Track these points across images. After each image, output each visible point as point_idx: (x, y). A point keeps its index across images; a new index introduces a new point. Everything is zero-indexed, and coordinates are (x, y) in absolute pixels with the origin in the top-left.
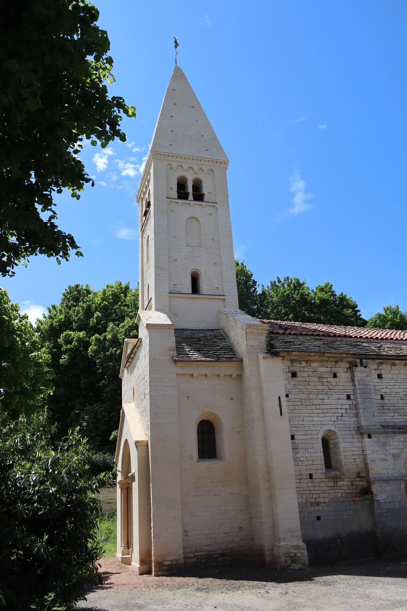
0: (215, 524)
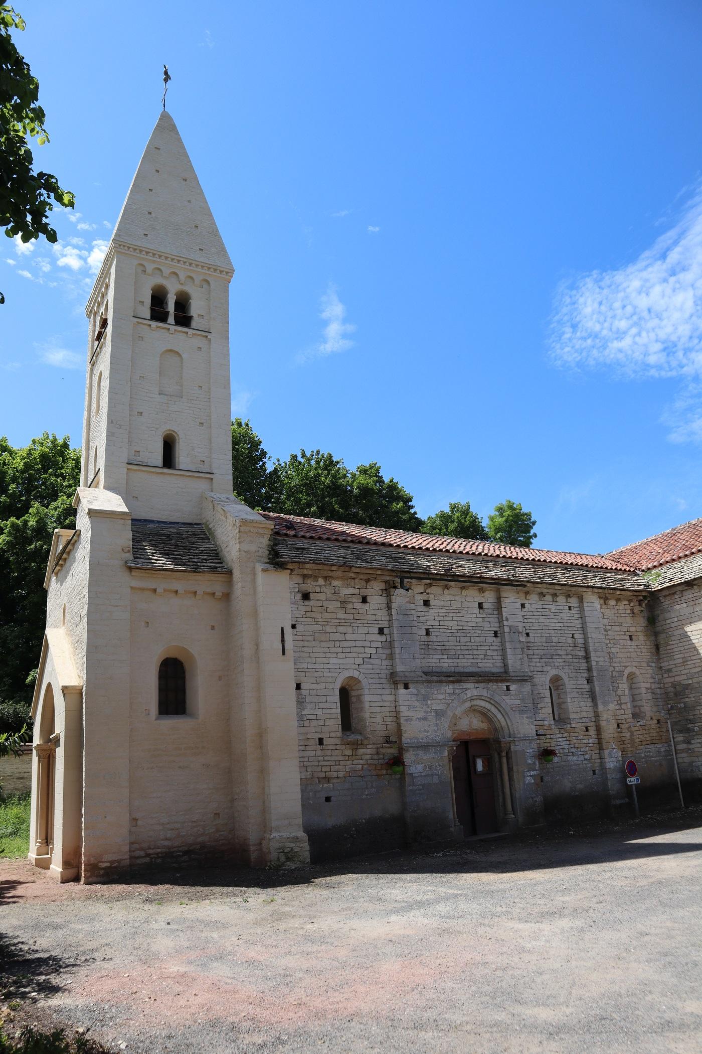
0: (178, 809)
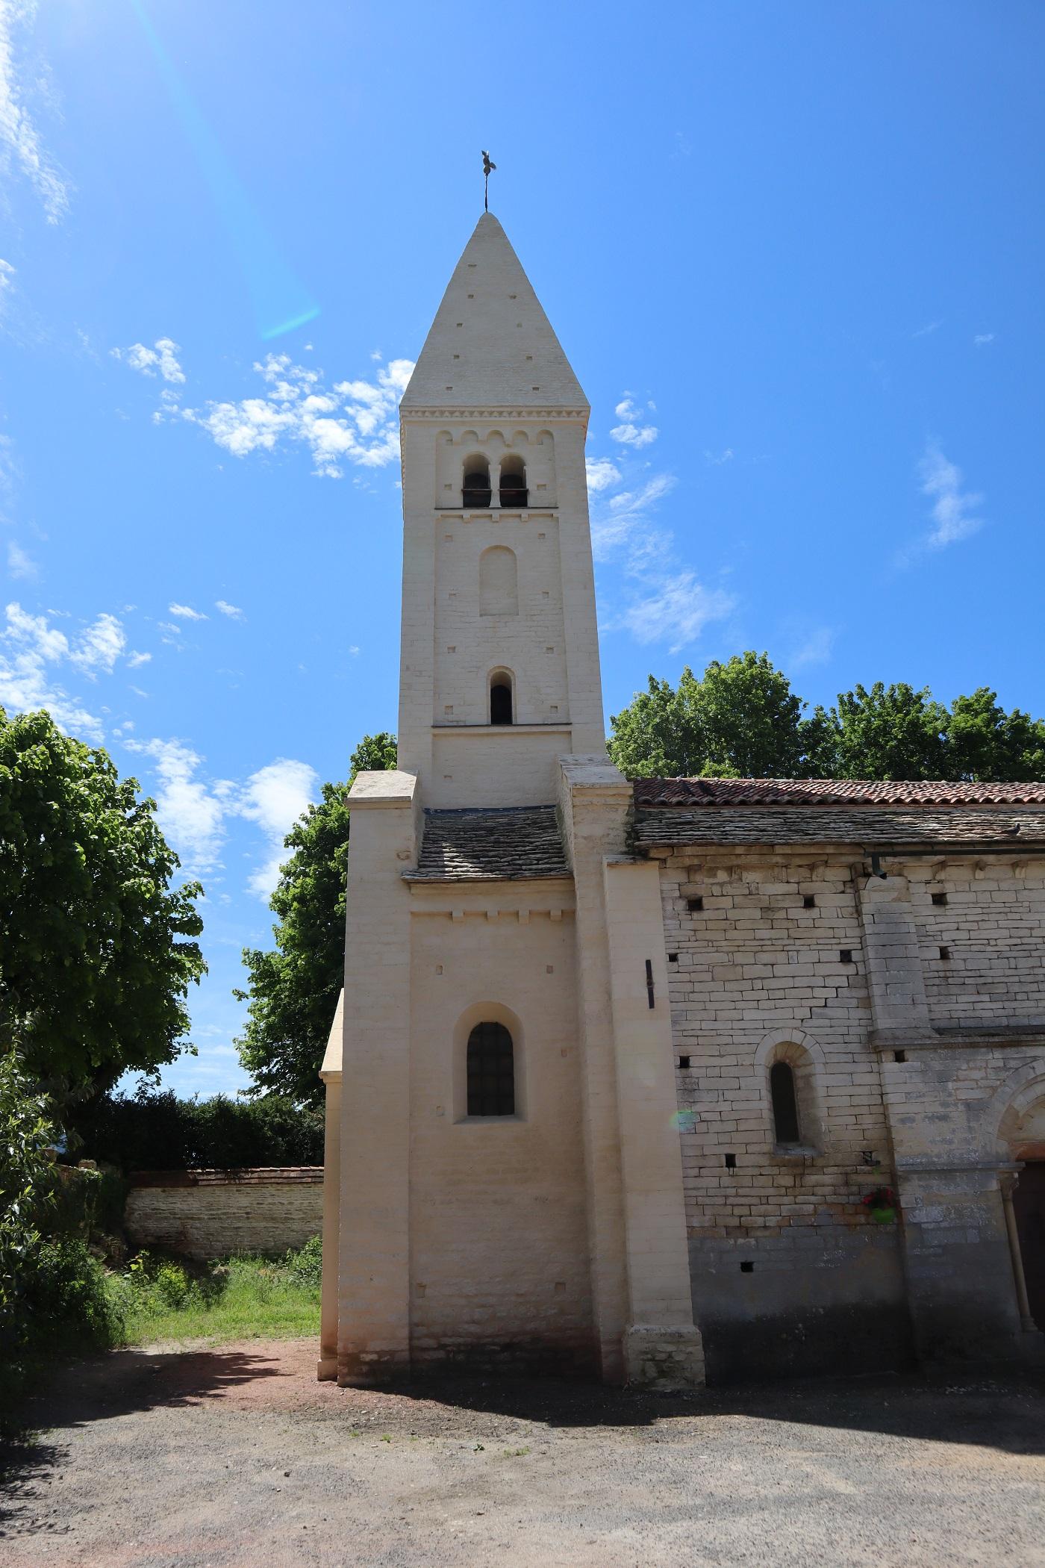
0: (487, 1271)
